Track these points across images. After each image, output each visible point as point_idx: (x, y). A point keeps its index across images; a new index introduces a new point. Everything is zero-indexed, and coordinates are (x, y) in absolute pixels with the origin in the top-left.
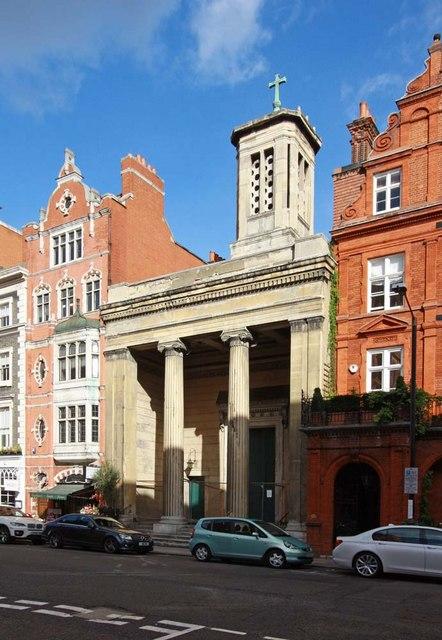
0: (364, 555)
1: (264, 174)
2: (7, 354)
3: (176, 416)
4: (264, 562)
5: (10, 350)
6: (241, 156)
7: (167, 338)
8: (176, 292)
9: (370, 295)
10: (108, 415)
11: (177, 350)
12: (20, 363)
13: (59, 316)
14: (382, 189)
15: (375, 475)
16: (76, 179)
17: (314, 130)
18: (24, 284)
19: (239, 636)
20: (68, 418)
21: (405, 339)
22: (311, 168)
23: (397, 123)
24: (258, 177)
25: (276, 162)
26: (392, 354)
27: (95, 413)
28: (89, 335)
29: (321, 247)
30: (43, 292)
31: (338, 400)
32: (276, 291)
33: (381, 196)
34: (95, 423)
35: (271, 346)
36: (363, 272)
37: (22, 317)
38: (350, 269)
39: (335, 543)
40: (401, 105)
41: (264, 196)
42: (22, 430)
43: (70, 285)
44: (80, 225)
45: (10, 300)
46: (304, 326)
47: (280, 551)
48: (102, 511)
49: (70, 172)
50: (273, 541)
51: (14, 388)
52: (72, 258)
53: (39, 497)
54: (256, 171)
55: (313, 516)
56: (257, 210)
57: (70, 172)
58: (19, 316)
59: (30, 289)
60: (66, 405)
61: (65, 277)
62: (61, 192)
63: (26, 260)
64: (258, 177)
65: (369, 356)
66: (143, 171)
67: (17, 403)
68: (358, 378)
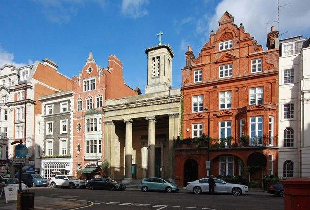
0: (197, 187)
1: (157, 64)
2: (66, 121)
3: (116, 142)
4: (232, 194)
5: (67, 120)
6: (149, 57)
7: (127, 118)
8: (130, 103)
9: (193, 107)
10: (105, 144)
11: (130, 122)
12: (71, 125)
13: (86, 109)
14: (197, 75)
15: (197, 165)
16: (93, 62)
17: (172, 51)
18: (73, 97)
19: (194, 209)
20: (90, 144)
21: (205, 121)
22: (171, 62)
23: (201, 55)
24: (154, 65)
25: (161, 61)
26: (200, 126)
27: (100, 143)
28: (99, 116)
29: (177, 92)
30: (80, 100)
31: (185, 140)
32: (164, 105)
33: (196, 77)
34: (100, 146)
35: (162, 122)
36: (191, 100)
37: (72, 108)
38: (187, 99)
39: (187, 184)
40: (202, 50)
41: (157, 71)
42: (71, 149)
43: (90, 98)
44: (95, 78)
45: (67, 102)
46: (173, 116)
47: (170, 187)
49: (91, 60)
50: (168, 184)
51: (68, 134)
52: (91, 89)
53: (78, 172)
54: (154, 63)
55: (177, 176)
56: (154, 76)
57: (91, 60)
58: (71, 108)
59: (75, 99)
60: (89, 140)
61: (89, 95)
62: (88, 66)
63: (74, 89)
64: (154, 65)
65: (193, 126)
66: (116, 61)
68: (189, 133)
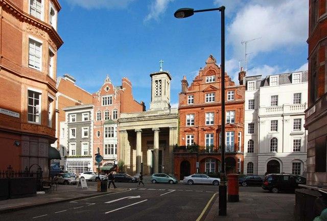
0: (190, 180)
1: (159, 86)
5: (88, 127)
7: (138, 128)
9: (187, 122)
18: (93, 109)
23: (193, 85)
27: (116, 147)
28: (115, 126)
30: (99, 112)
33: (189, 100)
35: (164, 132)
37: (92, 118)
38: (182, 116)
44: (112, 96)
47: (172, 180)
48: (142, 164)
59: (95, 111)
63: (93, 103)
65: (187, 136)
67: (90, 143)
68: (184, 141)
